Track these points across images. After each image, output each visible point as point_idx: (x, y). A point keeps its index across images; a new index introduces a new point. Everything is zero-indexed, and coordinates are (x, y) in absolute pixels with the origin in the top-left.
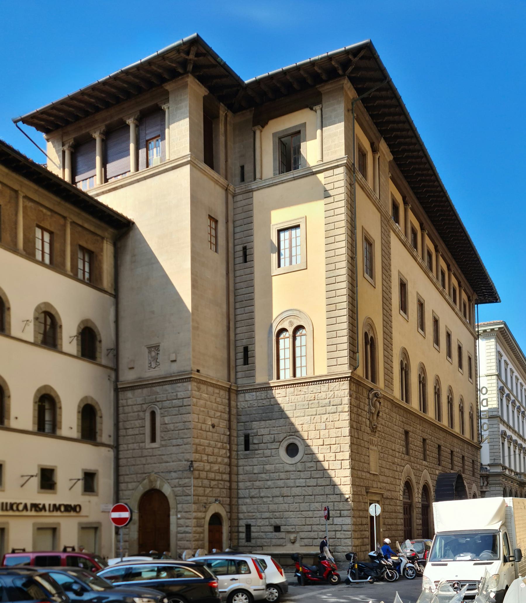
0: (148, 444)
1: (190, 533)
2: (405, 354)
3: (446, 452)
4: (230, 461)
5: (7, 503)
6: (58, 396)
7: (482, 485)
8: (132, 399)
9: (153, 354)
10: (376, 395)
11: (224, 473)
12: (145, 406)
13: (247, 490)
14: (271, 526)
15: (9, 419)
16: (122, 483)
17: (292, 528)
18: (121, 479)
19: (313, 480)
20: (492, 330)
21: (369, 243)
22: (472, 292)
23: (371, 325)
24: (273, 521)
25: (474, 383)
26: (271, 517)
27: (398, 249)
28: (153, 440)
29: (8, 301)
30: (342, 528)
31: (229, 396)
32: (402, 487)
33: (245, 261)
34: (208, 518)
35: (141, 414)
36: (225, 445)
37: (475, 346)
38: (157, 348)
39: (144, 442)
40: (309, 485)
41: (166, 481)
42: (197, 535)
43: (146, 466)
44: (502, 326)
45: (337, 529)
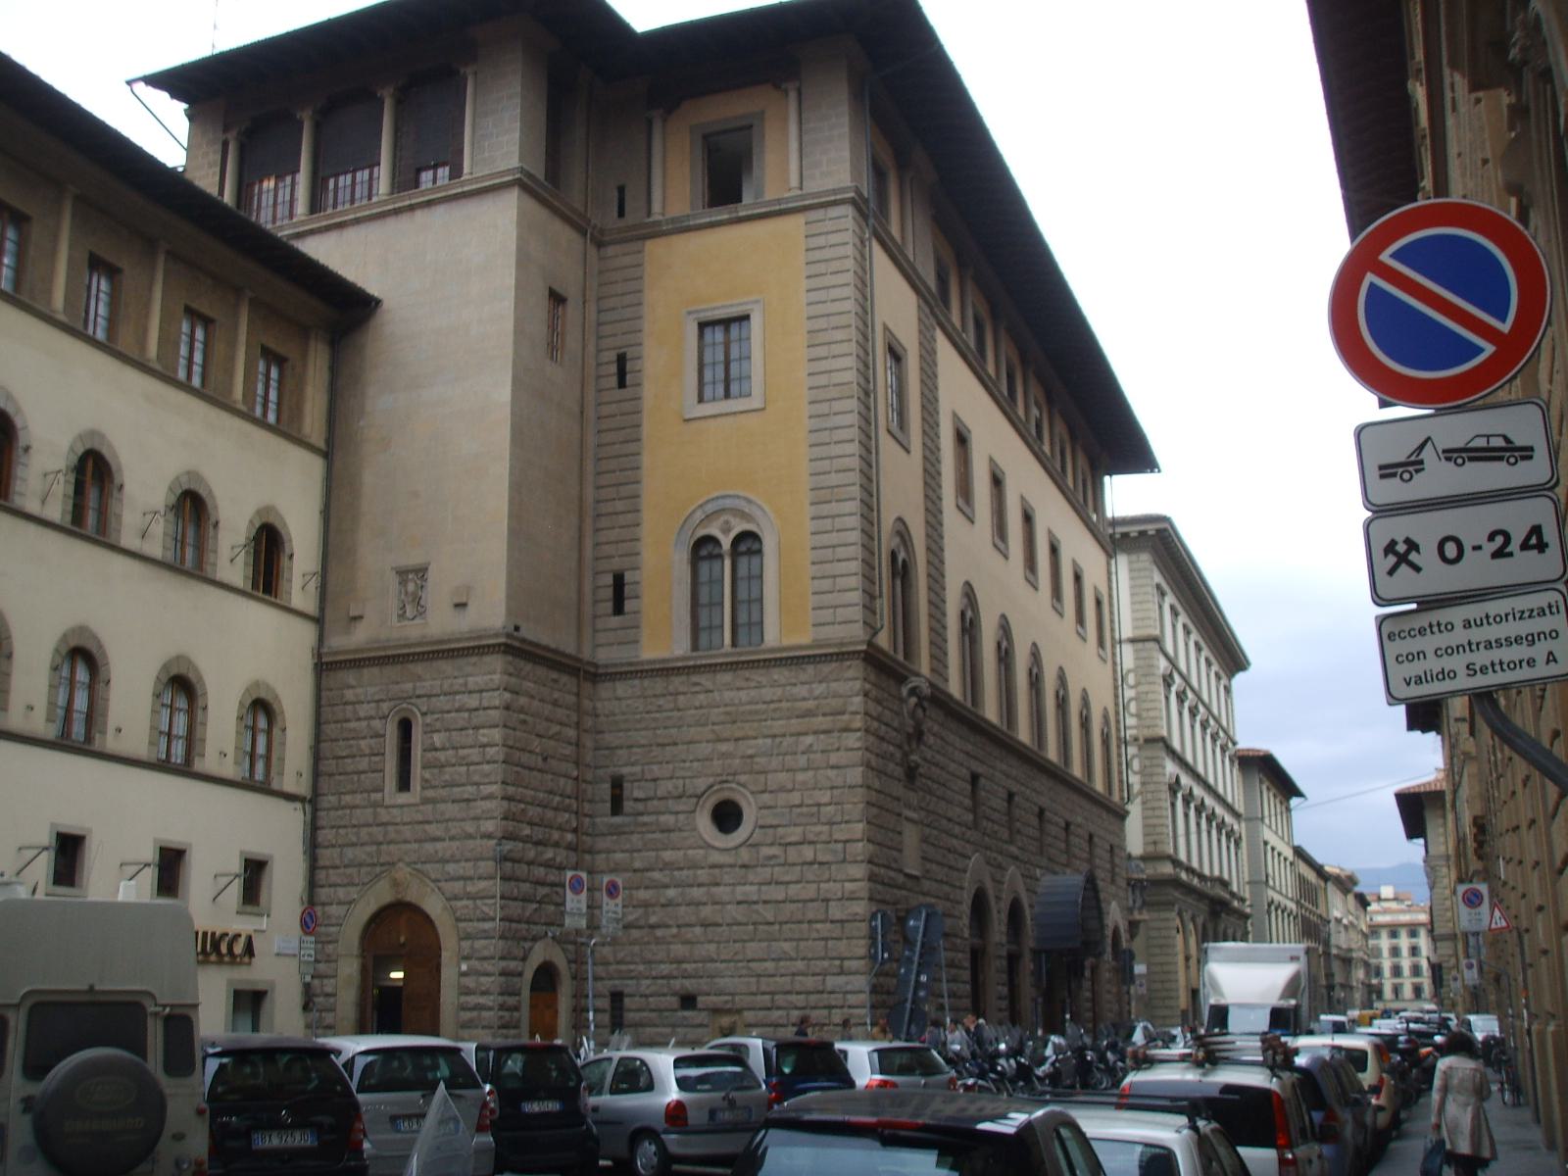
0: (390, 793)
1: (490, 1009)
2: (969, 593)
3: (1057, 824)
5: (205, 934)
6: (200, 678)
7: (1131, 902)
8: (364, 687)
9: (411, 587)
12: (385, 706)
14: (674, 994)
15: (104, 732)
16: (322, 886)
17: (726, 1002)
18: (321, 875)
20: (1142, 533)
21: (895, 355)
23: (903, 533)
24: (677, 984)
26: (675, 973)
27: (951, 368)
28: (404, 784)
29: (120, 469)
30: (845, 999)
32: (965, 908)
33: (622, 384)
34: (529, 975)
35: (377, 724)
36: (567, 801)
37: (1109, 573)
38: (421, 571)
39: (382, 790)
41: (432, 885)
42: (506, 1014)
43: (384, 847)
45: (833, 1003)
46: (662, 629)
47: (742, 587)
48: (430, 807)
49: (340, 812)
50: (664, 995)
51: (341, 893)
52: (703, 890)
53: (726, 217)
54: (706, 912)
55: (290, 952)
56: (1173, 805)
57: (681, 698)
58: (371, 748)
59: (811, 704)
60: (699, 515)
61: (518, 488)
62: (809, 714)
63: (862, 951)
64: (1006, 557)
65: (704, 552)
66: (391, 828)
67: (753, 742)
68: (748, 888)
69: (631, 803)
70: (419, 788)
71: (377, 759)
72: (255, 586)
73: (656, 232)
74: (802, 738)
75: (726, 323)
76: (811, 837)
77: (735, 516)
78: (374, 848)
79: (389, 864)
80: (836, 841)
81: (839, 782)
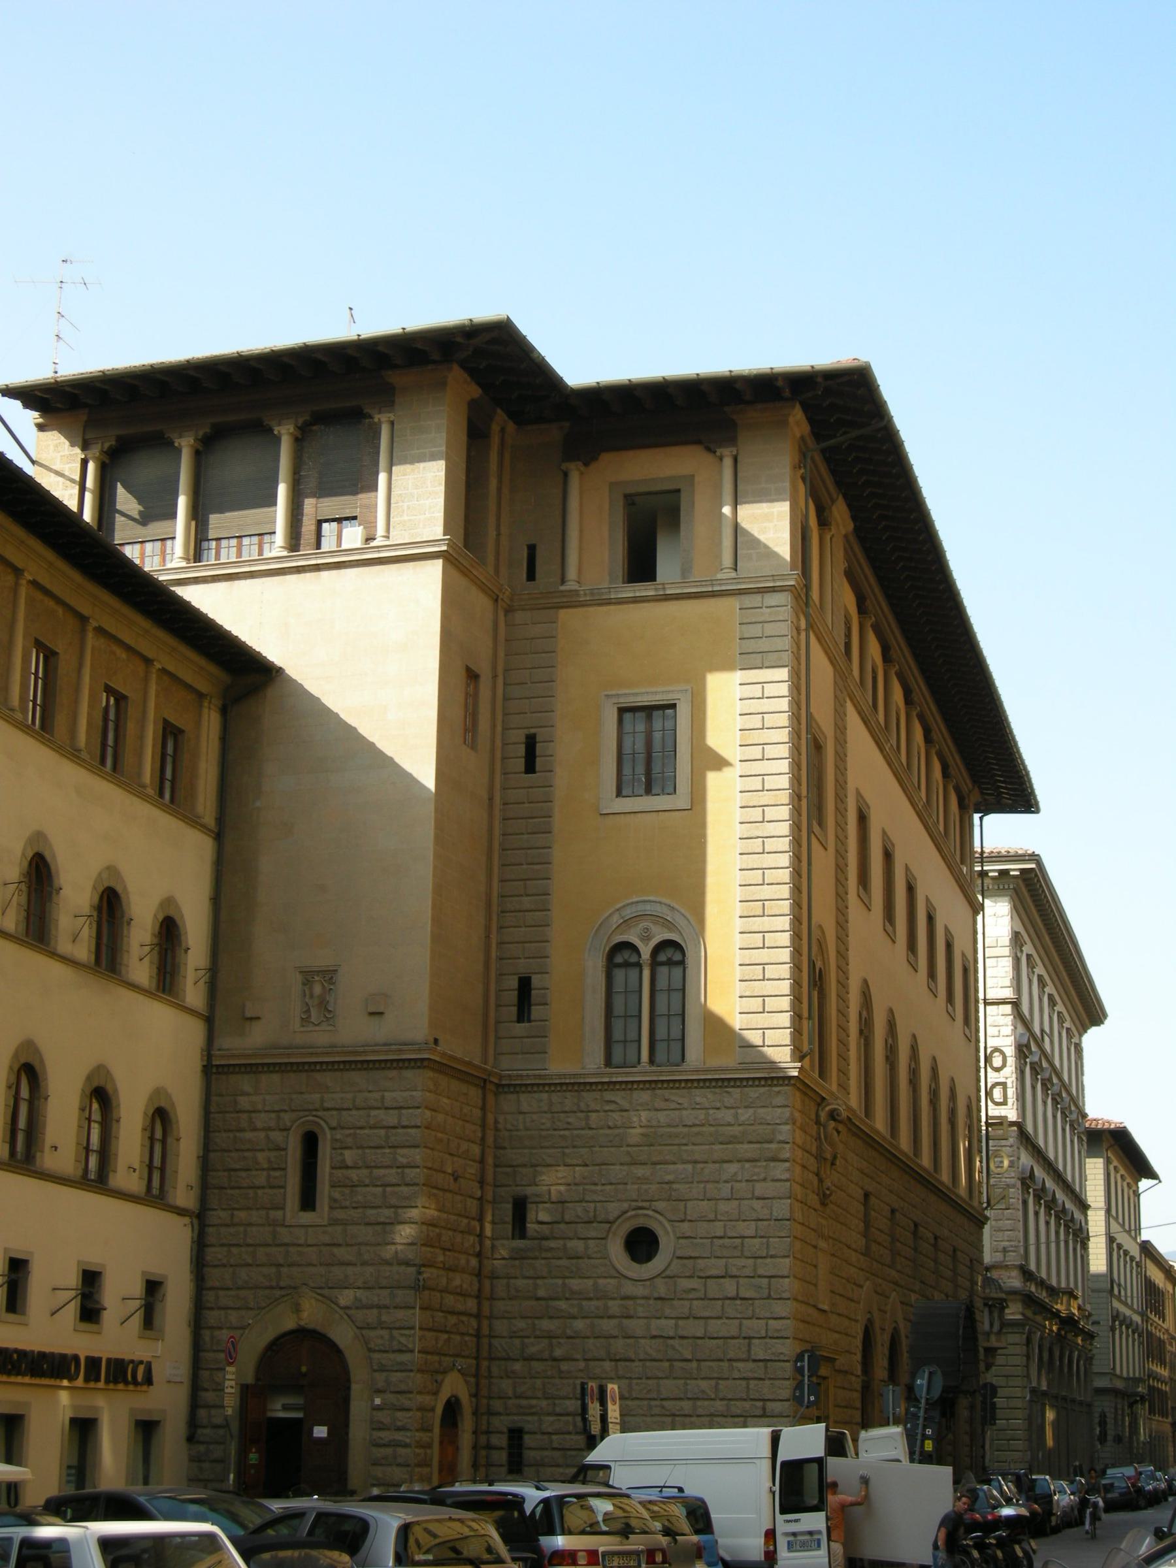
1: (406, 1446)
4: (480, 1263)
10: (833, 1115)
11: (470, 1296)
13: (517, 1341)
16: (212, 1309)
19: (696, 1322)
20: (1004, 873)
22: (970, 786)
25: (973, 1040)
28: (308, 1201)
31: (484, 1099)
35: (277, 1136)
38: (329, 975)
40: (685, 1333)
41: (341, 1312)
43: (284, 1270)
44: (1033, 866)
46: (573, 1041)
47: (662, 999)
48: (339, 1229)
49: (232, 1230)
50: (570, 1433)
51: (233, 1317)
52: (614, 1322)
53: (652, 593)
54: (619, 1346)
55: (178, 1379)
56: (1025, 1203)
57: (593, 1115)
58: (270, 1162)
59: (736, 1130)
60: (616, 920)
61: (439, 890)
62: (733, 1140)
63: (786, 1393)
64: (894, 942)
65: (619, 959)
66: (292, 1249)
67: (672, 1167)
68: (663, 1322)
69: (536, 1226)
70: (326, 1208)
71: (277, 1174)
72: (158, 989)
73: (573, 601)
74: (725, 1165)
75: (649, 710)
76: (734, 1271)
77: (655, 923)
78: (273, 1270)
79: (290, 1287)
80: (760, 1276)
81: (764, 1214)
